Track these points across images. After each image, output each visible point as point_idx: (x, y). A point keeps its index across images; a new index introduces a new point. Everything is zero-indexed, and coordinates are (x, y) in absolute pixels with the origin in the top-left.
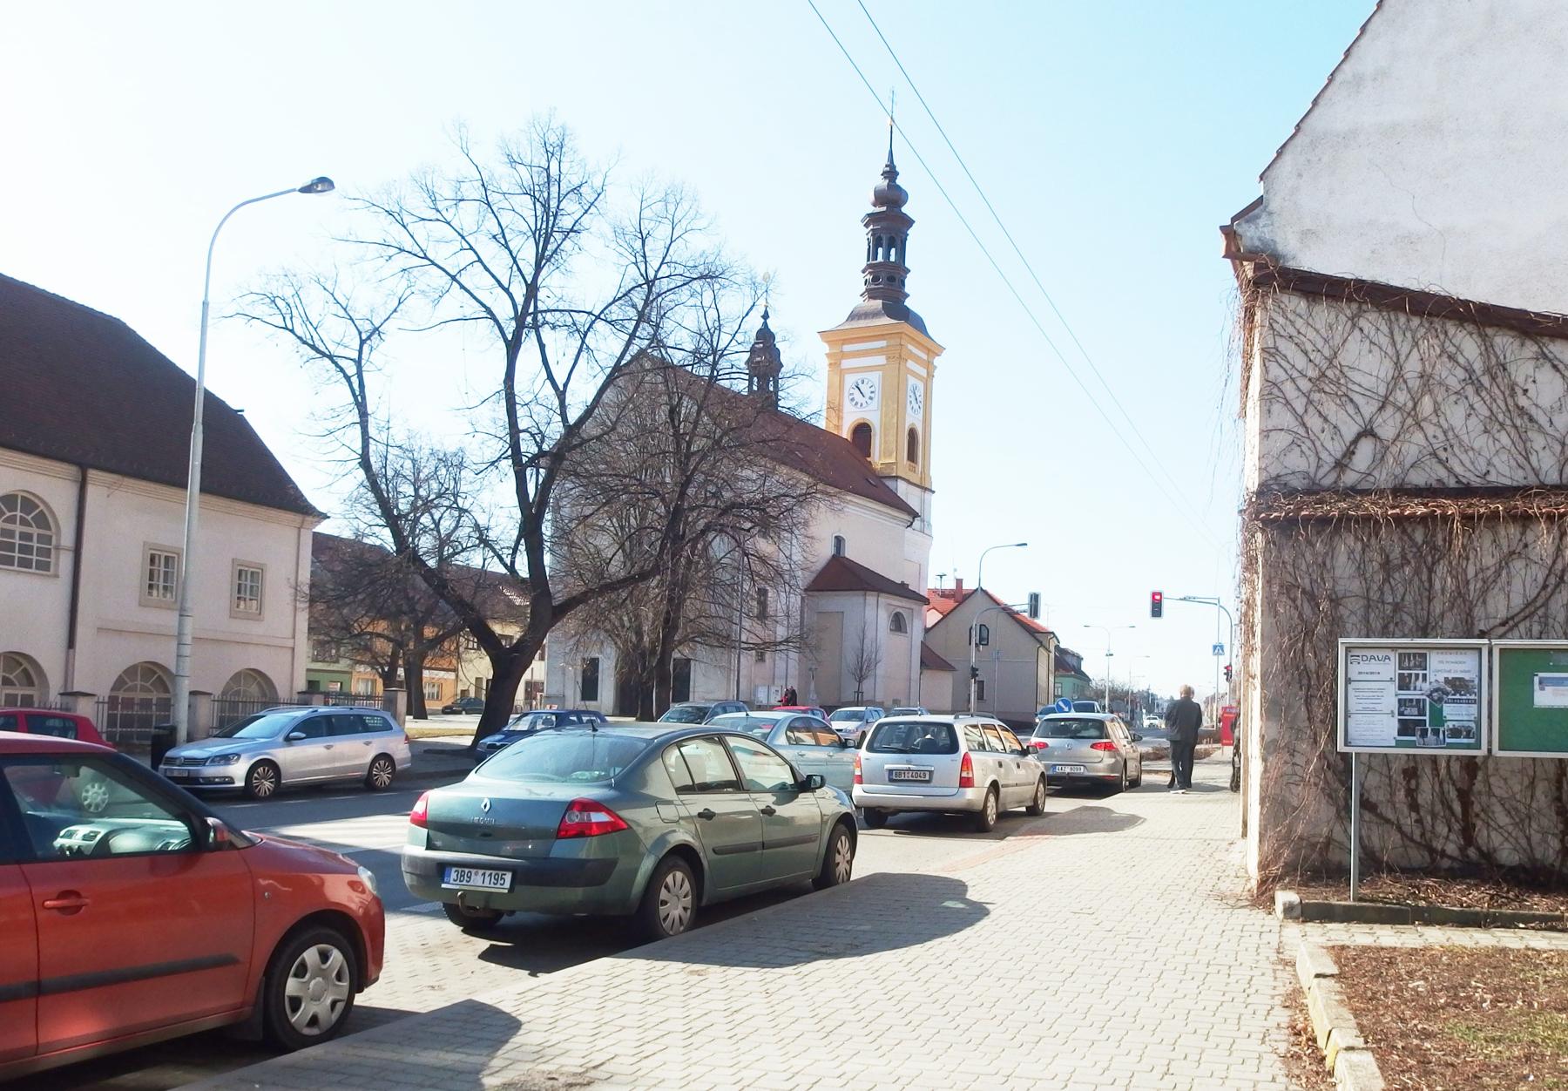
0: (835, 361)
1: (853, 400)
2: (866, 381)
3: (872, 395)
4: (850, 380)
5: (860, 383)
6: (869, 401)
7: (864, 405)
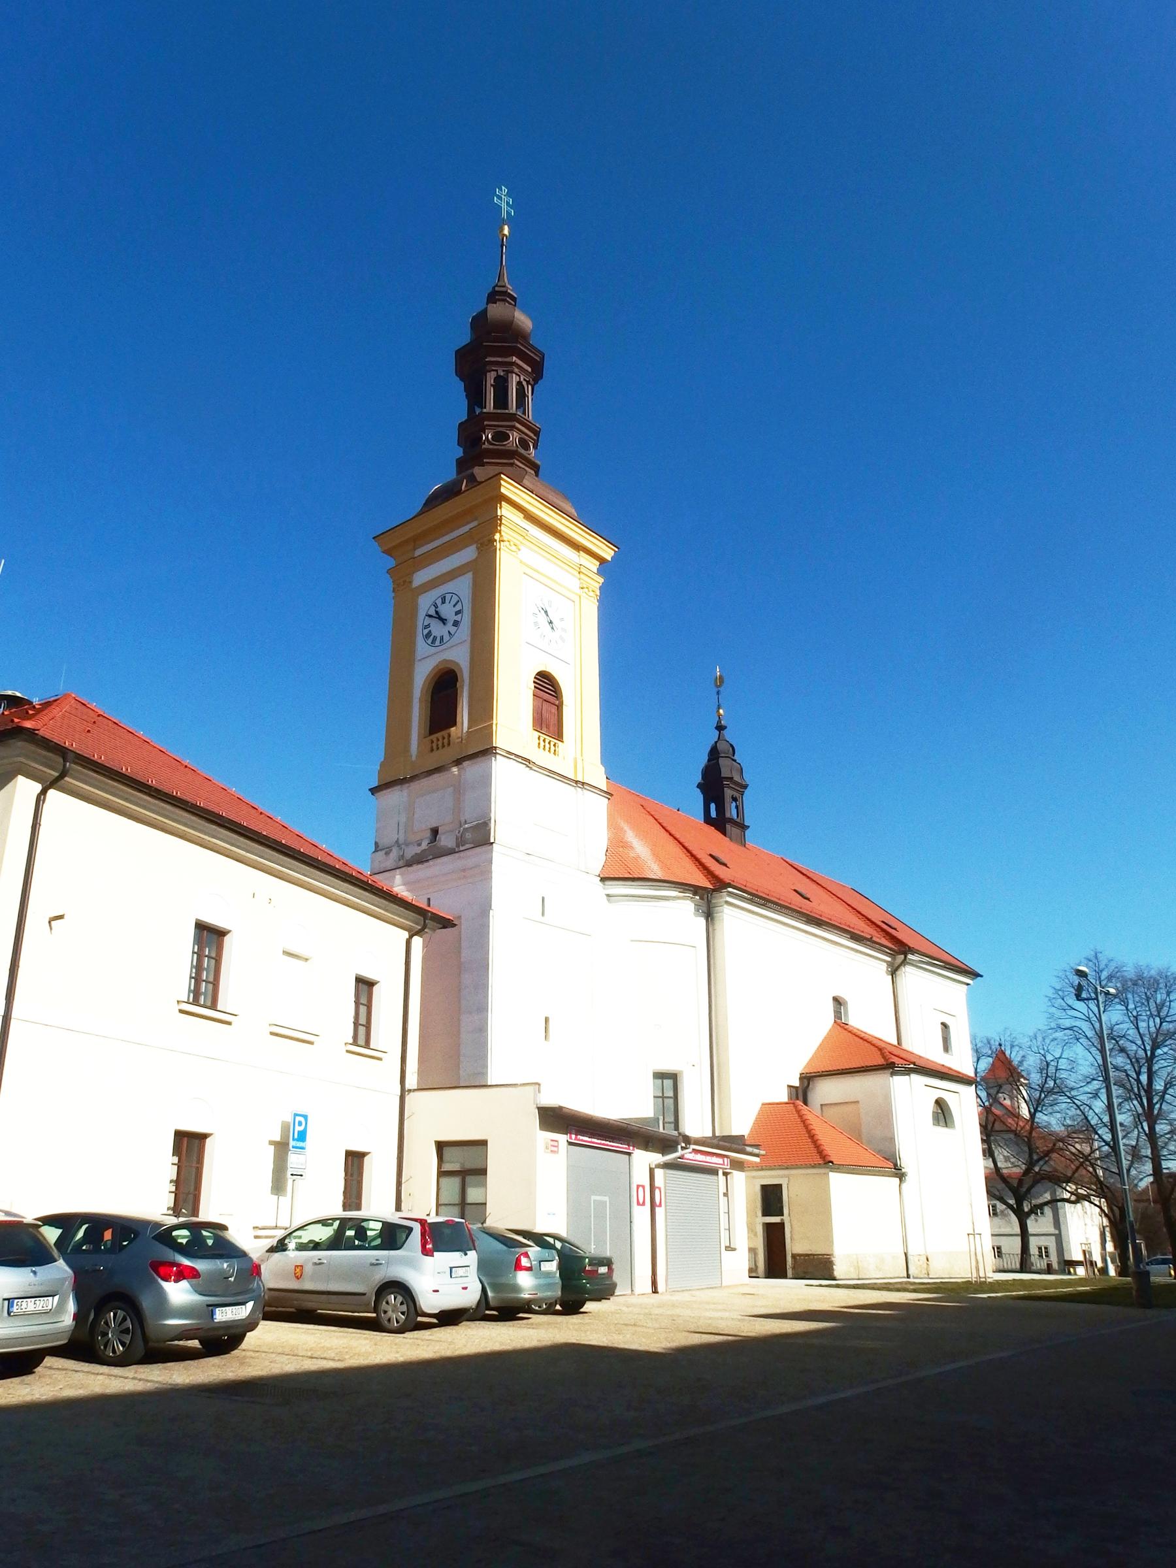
0: (401, 579)
1: (429, 634)
2: (448, 597)
3: (458, 618)
4: (425, 603)
5: (439, 602)
6: (453, 629)
7: (446, 637)
